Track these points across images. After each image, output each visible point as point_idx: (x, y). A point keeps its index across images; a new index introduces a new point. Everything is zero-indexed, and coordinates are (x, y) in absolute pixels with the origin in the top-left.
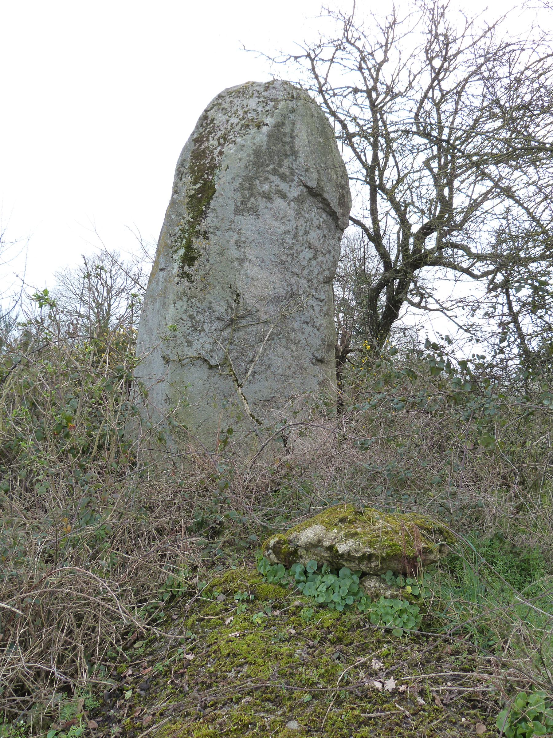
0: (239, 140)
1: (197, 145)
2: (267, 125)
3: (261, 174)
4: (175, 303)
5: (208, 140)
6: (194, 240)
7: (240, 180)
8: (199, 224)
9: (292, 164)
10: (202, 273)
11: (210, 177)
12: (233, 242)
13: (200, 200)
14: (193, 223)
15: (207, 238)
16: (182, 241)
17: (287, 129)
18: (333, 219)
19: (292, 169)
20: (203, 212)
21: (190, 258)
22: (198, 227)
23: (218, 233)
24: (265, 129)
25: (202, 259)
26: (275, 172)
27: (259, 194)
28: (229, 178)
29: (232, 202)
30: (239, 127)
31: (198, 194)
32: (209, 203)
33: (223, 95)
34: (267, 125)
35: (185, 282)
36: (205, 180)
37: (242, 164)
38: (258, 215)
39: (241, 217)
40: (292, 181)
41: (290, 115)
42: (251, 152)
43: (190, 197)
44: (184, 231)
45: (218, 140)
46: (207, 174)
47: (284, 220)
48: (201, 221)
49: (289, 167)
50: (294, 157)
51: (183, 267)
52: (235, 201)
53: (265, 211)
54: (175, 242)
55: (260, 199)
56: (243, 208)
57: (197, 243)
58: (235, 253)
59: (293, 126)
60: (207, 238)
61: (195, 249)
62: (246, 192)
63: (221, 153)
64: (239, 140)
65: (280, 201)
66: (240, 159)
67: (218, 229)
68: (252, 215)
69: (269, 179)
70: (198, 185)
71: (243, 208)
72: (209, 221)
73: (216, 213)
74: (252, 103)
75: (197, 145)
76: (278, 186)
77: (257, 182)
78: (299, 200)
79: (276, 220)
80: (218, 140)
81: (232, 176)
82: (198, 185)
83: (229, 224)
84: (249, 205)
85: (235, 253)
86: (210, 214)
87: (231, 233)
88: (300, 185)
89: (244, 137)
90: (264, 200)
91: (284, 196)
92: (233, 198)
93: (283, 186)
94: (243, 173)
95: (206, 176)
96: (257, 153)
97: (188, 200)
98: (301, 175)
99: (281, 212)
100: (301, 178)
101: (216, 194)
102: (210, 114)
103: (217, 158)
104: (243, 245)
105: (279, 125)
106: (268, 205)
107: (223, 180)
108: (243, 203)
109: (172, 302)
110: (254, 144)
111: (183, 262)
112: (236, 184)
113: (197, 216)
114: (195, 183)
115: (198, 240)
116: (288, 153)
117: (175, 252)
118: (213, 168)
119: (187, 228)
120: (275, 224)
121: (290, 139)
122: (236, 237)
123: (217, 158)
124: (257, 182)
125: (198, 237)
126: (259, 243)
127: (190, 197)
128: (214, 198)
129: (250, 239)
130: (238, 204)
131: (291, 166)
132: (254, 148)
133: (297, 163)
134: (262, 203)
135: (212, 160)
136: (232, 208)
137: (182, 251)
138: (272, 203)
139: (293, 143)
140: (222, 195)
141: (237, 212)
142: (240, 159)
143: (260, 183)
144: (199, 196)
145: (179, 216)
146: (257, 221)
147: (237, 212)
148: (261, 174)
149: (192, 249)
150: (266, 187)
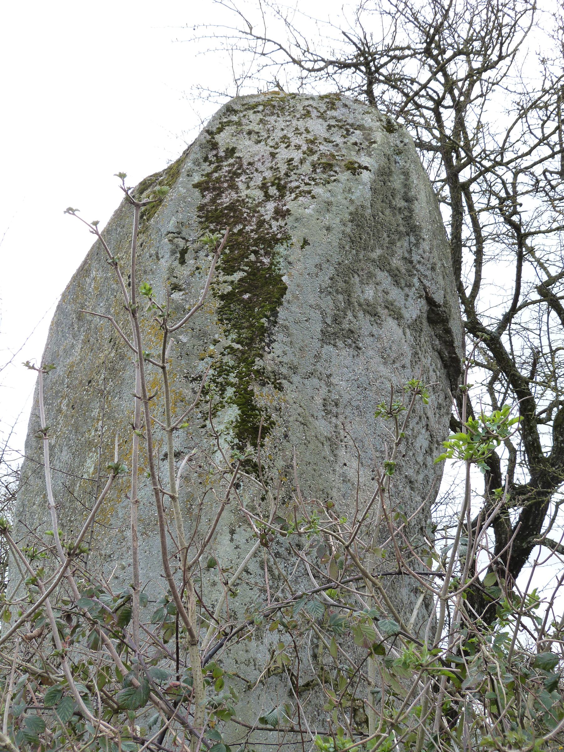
0: (318, 190)
1: (209, 196)
2: (366, 168)
3: (362, 265)
4: (232, 532)
5: (233, 187)
6: (256, 388)
7: (331, 271)
8: (261, 356)
9: (410, 252)
10: (280, 463)
11: (266, 260)
12: (319, 401)
13: (248, 306)
14: (243, 353)
15: (280, 388)
16: (223, 391)
17: (397, 182)
18: (448, 376)
19: (411, 262)
20: (263, 330)
21: (251, 429)
22: (259, 363)
23: (296, 379)
24: (366, 176)
25: (278, 432)
26: (383, 264)
27: (360, 305)
28: (311, 263)
29: (316, 315)
30: (307, 168)
31: (242, 293)
32: (275, 314)
33: (236, 108)
34: (366, 168)
35: (252, 485)
36: (250, 264)
37: (334, 238)
38: (358, 348)
39: (331, 348)
40: (410, 286)
41: (398, 158)
42: (348, 217)
43: (222, 297)
44: (222, 370)
45: (264, 187)
46: (256, 253)
47: (397, 365)
48: (263, 348)
49: (405, 258)
50: (413, 239)
51: (241, 449)
52: (323, 314)
53: (369, 340)
54: (205, 392)
55: (360, 314)
56: (337, 332)
57: (263, 396)
58: (323, 427)
59: (407, 179)
60: (280, 388)
61: (260, 410)
62: (340, 297)
63: (280, 214)
64: (318, 190)
65: (391, 323)
66: (328, 229)
67: (294, 369)
68: (350, 346)
69: (375, 276)
70: (237, 276)
71: (337, 332)
72: (276, 354)
73: (289, 335)
74: (318, 127)
75: (209, 196)
76: (387, 293)
77: (357, 279)
78: (415, 327)
79: (385, 363)
80: (264, 187)
81: (317, 260)
82: (237, 276)
83: (313, 361)
84: (346, 326)
85: (323, 427)
86: (280, 337)
87: (315, 381)
88: (420, 297)
89: (329, 187)
90: (368, 317)
91: (398, 317)
92: (318, 307)
93: (395, 294)
94: (336, 258)
95: (252, 257)
96: (356, 218)
97: (218, 303)
98: (426, 276)
99: (394, 347)
100: (425, 281)
101: (288, 296)
102: (223, 139)
103: (274, 223)
104: (334, 410)
105: (384, 174)
106: (375, 330)
107: (299, 266)
108: (336, 320)
109: (226, 530)
110: (352, 201)
111: (239, 435)
112: (324, 280)
113: (252, 339)
114: (229, 271)
115: (265, 390)
116: (402, 229)
117: (214, 413)
118: (269, 242)
119: (231, 363)
120: (384, 370)
121: (403, 204)
122: (324, 391)
123: (274, 223)
124: (357, 279)
125: (263, 384)
126: (358, 408)
127: (222, 297)
128: (285, 304)
129: (346, 397)
130: (329, 321)
131: (406, 255)
132: (352, 209)
133: (420, 251)
134: (364, 324)
135: (261, 223)
136: (318, 327)
137: (232, 413)
138: (380, 325)
139: (411, 211)
140: (297, 298)
141: (327, 337)
142: (328, 229)
143: (361, 282)
144: (246, 296)
145: (199, 338)
146: (357, 360)
147: (327, 337)
148: (362, 265)
149: (254, 408)
150: (369, 293)
